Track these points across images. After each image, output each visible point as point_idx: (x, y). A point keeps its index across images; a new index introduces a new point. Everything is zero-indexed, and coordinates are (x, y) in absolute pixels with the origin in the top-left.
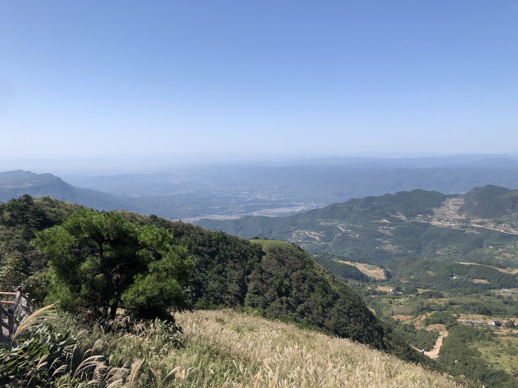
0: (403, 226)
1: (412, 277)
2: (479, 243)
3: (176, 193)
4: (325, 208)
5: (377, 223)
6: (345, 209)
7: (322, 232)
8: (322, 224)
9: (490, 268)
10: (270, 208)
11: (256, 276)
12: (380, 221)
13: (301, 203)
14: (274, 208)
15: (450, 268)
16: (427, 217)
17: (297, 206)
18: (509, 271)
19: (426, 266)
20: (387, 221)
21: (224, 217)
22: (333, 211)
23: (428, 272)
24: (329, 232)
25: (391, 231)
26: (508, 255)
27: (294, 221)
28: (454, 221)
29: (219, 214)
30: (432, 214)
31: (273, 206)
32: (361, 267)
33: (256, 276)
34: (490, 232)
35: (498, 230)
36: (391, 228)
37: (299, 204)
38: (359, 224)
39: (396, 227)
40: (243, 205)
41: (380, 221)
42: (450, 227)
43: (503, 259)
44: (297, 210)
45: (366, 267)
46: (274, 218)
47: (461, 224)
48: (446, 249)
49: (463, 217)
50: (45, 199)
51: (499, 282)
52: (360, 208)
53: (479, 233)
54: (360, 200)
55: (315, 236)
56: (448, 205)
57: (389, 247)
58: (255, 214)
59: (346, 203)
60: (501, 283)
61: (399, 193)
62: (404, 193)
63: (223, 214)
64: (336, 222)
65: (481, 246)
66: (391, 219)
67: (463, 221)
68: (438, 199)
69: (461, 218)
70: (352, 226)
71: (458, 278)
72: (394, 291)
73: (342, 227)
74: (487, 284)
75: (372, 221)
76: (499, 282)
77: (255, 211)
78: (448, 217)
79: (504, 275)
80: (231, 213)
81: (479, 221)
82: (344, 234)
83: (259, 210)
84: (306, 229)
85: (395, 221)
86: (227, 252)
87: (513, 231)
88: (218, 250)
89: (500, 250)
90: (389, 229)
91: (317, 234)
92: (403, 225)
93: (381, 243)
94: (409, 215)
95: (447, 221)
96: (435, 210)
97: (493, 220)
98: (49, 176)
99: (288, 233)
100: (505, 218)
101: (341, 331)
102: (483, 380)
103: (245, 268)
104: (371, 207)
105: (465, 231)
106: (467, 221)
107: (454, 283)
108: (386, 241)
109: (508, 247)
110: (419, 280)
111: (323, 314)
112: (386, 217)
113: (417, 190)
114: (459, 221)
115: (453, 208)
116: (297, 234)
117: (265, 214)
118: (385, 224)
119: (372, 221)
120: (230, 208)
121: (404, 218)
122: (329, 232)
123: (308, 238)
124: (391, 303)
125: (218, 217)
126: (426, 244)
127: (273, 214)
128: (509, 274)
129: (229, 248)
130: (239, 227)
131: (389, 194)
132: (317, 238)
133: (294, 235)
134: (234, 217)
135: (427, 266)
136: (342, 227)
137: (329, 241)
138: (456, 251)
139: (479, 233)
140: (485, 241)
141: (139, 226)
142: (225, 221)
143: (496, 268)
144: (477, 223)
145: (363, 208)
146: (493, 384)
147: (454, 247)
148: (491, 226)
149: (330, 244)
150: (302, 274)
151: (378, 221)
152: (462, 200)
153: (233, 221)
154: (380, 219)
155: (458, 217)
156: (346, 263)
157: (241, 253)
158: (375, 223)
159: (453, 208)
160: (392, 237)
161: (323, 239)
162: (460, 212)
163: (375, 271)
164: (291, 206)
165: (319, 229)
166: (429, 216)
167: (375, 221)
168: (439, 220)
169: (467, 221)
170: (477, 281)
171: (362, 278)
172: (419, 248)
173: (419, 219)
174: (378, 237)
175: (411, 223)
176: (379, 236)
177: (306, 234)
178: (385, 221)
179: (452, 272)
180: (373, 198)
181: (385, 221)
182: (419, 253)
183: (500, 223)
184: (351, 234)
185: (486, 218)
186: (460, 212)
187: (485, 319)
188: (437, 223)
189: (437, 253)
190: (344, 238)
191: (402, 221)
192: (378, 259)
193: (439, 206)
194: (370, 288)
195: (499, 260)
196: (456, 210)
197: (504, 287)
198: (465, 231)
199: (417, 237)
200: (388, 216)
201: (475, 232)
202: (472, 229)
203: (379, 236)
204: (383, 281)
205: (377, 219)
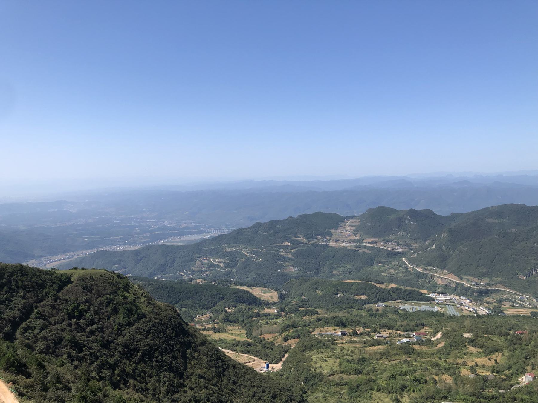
1: (303, 297)
2: (370, 262)
3: (72, 223)
5: (279, 246)
6: (250, 233)
7: (226, 258)
8: (227, 249)
9: (369, 285)
10: (178, 236)
11: (48, 303)
13: (212, 229)
14: (183, 235)
15: (335, 286)
16: (326, 239)
17: (208, 232)
18: (386, 286)
19: (315, 286)
20: (289, 244)
21: (126, 248)
22: (238, 236)
23: (317, 292)
24: (234, 257)
26: (393, 271)
27: (199, 248)
28: (349, 241)
30: (331, 235)
31: (182, 233)
32: (256, 292)
33: (48, 303)
34: (380, 250)
35: (386, 248)
40: (148, 234)
42: (345, 247)
43: (389, 275)
44: (208, 236)
45: (262, 290)
46: (178, 247)
47: (356, 244)
49: (358, 237)
50: (290, 217)
51: (376, 296)
53: (370, 252)
54: (264, 224)
55: (220, 262)
56: (345, 227)
57: (290, 270)
58: (161, 243)
59: (251, 228)
60: (377, 297)
61: (300, 216)
62: (306, 216)
63: (124, 245)
65: (372, 264)
67: (357, 241)
68: (336, 221)
69: (355, 238)
70: (256, 251)
71: (343, 295)
72: (278, 312)
74: (366, 300)
75: (275, 245)
76: (376, 296)
77: (161, 239)
78: (344, 238)
79: (379, 290)
80: (134, 243)
81: (370, 240)
83: (165, 238)
84: (211, 255)
86: (20, 283)
87: (398, 248)
88: (10, 281)
89: (387, 267)
90: (291, 252)
92: (303, 247)
93: (282, 266)
96: (333, 231)
97: (382, 239)
99: (191, 261)
100: (392, 237)
101: (132, 345)
102: (306, 382)
103: (38, 297)
104: (274, 231)
105: (358, 251)
106: (361, 241)
107: (338, 301)
108: (287, 264)
109: (393, 263)
110: (308, 300)
111: (118, 332)
114: (354, 241)
115: (348, 229)
116: (201, 261)
118: (288, 246)
119: (275, 245)
120: (133, 237)
121: (305, 240)
122: (234, 257)
123: (212, 265)
124: (268, 324)
125: (118, 248)
127: (181, 241)
128: (384, 289)
129: (24, 279)
130: (139, 258)
131: (292, 217)
132: (222, 265)
133: (198, 263)
134: (136, 247)
135: (316, 286)
137: (233, 267)
139: (370, 252)
140: (376, 259)
142: (124, 252)
143: (375, 284)
144: (369, 243)
146: (312, 385)
148: (380, 245)
149: (234, 270)
150: (107, 299)
152: (358, 221)
153: (132, 252)
154: (282, 242)
155: (353, 237)
156: (242, 288)
157: (37, 284)
158: (277, 247)
159: (348, 229)
161: (227, 265)
163: (270, 294)
165: (223, 255)
166: (327, 238)
167: (278, 245)
168: (337, 241)
169: (361, 241)
170: (357, 297)
171: (255, 302)
172: (318, 269)
173: (319, 240)
174: (280, 260)
175: (311, 244)
178: (287, 243)
179: (337, 291)
181: (287, 243)
182: (318, 274)
183: (388, 242)
185: (377, 237)
186: (355, 232)
187: (335, 330)
189: (333, 273)
190: (248, 262)
191: (302, 243)
192: (277, 282)
193: (337, 228)
194: (256, 311)
195: (385, 276)
197: (381, 301)
198: (358, 251)
199: (316, 258)
200: (290, 238)
201: (367, 251)
203: (280, 259)
204: (275, 303)
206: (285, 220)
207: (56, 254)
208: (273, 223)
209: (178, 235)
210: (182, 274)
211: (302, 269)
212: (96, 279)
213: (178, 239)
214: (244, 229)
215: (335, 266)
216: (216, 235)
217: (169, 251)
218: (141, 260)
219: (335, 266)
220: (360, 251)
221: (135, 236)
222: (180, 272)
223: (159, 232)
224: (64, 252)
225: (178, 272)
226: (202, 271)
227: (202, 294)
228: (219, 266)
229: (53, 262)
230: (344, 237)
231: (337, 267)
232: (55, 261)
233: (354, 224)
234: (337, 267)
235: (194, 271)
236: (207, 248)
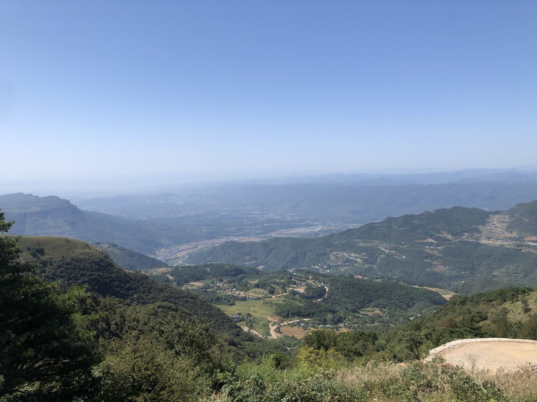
0: (451, 246)
4: (361, 227)
7: (363, 254)
8: (361, 244)
10: (287, 228)
12: (425, 241)
13: (318, 223)
14: (292, 228)
17: (314, 225)
20: (433, 241)
22: (370, 231)
24: (372, 255)
25: (439, 251)
28: (506, 239)
29: (237, 236)
30: (479, 231)
31: (290, 226)
36: (439, 248)
37: (316, 223)
38: (403, 245)
39: (443, 247)
40: (260, 226)
41: (425, 241)
47: (514, 242)
48: (504, 269)
49: (514, 235)
50: (426, 212)
52: (400, 227)
54: (398, 218)
55: (356, 258)
56: (494, 223)
58: (274, 235)
62: (443, 211)
63: (240, 236)
64: (377, 242)
66: (436, 239)
68: (482, 217)
69: (512, 236)
73: (384, 248)
77: (272, 231)
82: (388, 255)
83: (276, 230)
84: (344, 251)
85: (442, 241)
90: (437, 249)
91: (358, 255)
94: (455, 234)
95: (498, 239)
98: (54, 199)
105: (521, 250)
106: (521, 239)
108: (435, 263)
112: (431, 236)
113: (454, 207)
114: (511, 239)
116: (335, 256)
117: (286, 234)
118: (431, 244)
120: (246, 229)
121: (450, 237)
122: (372, 255)
123: (348, 261)
126: (480, 265)
130: (269, 250)
131: (428, 212)
132: (359, 260)
136: (384, 248)
137: (372, 263)
138: (515, 272)
144: (533, 242)
145: (403, 227)
147: (512, 268)
149: (375, 267)
151: (423, 241)
159: (499, 225)
160: (441, 258)
161: (366, 261)
162: (510, 228)
164: (308, 226)
165: (359, 250)
168: (489, 238)
169: (521, 239)
172: (473, 269)
173: (466, 237)
174: (427, 257)
175: (459, 242)
177: (344, 256)
178: (430, 240)
180: (412, 217)
181: (430, 240)
182: (473, 274)
184: (396, 255)
186: (510, 228)
188: (487, 241)
191: (448, 240)
193: (484, 224)
196: (504, 227)
198: (521, 250)
201: (532, 251)
202: (529, 248)
205: (421, 239)
206: (421, 215)
207: (181, 244)
208: (408, 219)
209: (287, 227)
210: (318, 268)
211: (453, 268)
213: (302, 230)
215: (495, 266)
216: (301, 229)
217: (297, 243)
218: (270, 252)
219: (495, 266)
220: (523, 251)
221: (248, 227)
222: (314, 265)
224: (187, 242)
225: (312, 265)
226: (338, 266)
227: (391, 294)
228: (356, 262)
229: (181, 251)
230: (497, 235)
231: (497, 268)
232: (183, 250)
233: (504, 220)
234: (497, 268)
235: (330, 266)
236: (337, 242)
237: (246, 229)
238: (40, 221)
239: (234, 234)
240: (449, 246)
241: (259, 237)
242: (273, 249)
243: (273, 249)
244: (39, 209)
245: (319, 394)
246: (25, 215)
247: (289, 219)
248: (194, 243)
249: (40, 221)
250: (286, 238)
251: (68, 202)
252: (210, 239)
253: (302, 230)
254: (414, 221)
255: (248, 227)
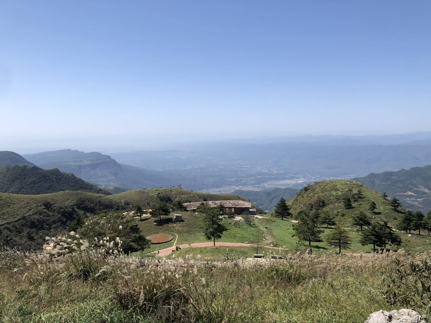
5: (403, 195)
10: (275, 180)
12: (405, 194)
20: (413, 194)
29: (237, 185)
31: (278, 178)
36: (418, 200)
39: (422, 199)
40: (253, 178)
41: (405, 194)
54: (379, 175)
61: (413, 169)
63: (239, 185)
66: (415, 192)
77: (264, 182)
83: (267, 182)
98: (96, 155)
112: (410, 190)
117: (274, 185)
118: (411, 196)
120: (243, 180)
121: (426, 191)
130: (271, 198)
131: (404, 170)
141: (258, 282)
145: (384, 182)
164: (291, 178)
176: (409, 207)
178: (410, 193)
181: (410, 193)
191: (426, 194)
200: (411, 189)
203: (409, 207)
209: (275, 179)
212: (277, 237)
213: (288, 182)
214: (360, 178)
218: (273, 200)
223: (260, 177)
237: (243, 180)
238: (92, 172)
239: (234, 184)
240: (427, 198)
241: (255, 187)
242: (275, 197)
243: (275, 197)
244: (89, 162)
245: (245, 281)
246: (80, 167)
247: (275, 172)
248: (205, 190)
249: (92, 172)
250: (285, 189)
251: (109, 157)
252: (217, 188)
253: (288, 182)
254: (394, 177)
255: (245, 179)
